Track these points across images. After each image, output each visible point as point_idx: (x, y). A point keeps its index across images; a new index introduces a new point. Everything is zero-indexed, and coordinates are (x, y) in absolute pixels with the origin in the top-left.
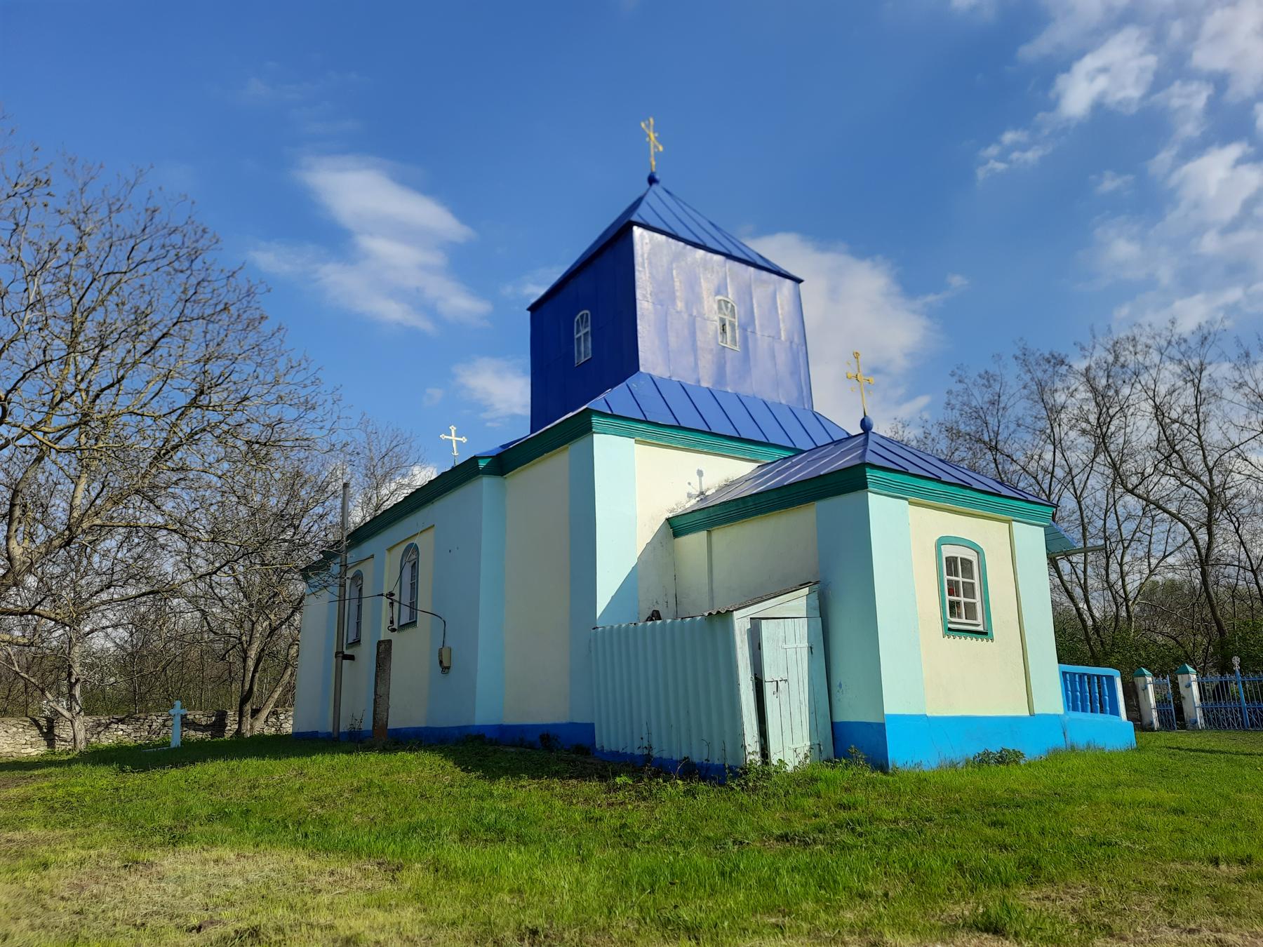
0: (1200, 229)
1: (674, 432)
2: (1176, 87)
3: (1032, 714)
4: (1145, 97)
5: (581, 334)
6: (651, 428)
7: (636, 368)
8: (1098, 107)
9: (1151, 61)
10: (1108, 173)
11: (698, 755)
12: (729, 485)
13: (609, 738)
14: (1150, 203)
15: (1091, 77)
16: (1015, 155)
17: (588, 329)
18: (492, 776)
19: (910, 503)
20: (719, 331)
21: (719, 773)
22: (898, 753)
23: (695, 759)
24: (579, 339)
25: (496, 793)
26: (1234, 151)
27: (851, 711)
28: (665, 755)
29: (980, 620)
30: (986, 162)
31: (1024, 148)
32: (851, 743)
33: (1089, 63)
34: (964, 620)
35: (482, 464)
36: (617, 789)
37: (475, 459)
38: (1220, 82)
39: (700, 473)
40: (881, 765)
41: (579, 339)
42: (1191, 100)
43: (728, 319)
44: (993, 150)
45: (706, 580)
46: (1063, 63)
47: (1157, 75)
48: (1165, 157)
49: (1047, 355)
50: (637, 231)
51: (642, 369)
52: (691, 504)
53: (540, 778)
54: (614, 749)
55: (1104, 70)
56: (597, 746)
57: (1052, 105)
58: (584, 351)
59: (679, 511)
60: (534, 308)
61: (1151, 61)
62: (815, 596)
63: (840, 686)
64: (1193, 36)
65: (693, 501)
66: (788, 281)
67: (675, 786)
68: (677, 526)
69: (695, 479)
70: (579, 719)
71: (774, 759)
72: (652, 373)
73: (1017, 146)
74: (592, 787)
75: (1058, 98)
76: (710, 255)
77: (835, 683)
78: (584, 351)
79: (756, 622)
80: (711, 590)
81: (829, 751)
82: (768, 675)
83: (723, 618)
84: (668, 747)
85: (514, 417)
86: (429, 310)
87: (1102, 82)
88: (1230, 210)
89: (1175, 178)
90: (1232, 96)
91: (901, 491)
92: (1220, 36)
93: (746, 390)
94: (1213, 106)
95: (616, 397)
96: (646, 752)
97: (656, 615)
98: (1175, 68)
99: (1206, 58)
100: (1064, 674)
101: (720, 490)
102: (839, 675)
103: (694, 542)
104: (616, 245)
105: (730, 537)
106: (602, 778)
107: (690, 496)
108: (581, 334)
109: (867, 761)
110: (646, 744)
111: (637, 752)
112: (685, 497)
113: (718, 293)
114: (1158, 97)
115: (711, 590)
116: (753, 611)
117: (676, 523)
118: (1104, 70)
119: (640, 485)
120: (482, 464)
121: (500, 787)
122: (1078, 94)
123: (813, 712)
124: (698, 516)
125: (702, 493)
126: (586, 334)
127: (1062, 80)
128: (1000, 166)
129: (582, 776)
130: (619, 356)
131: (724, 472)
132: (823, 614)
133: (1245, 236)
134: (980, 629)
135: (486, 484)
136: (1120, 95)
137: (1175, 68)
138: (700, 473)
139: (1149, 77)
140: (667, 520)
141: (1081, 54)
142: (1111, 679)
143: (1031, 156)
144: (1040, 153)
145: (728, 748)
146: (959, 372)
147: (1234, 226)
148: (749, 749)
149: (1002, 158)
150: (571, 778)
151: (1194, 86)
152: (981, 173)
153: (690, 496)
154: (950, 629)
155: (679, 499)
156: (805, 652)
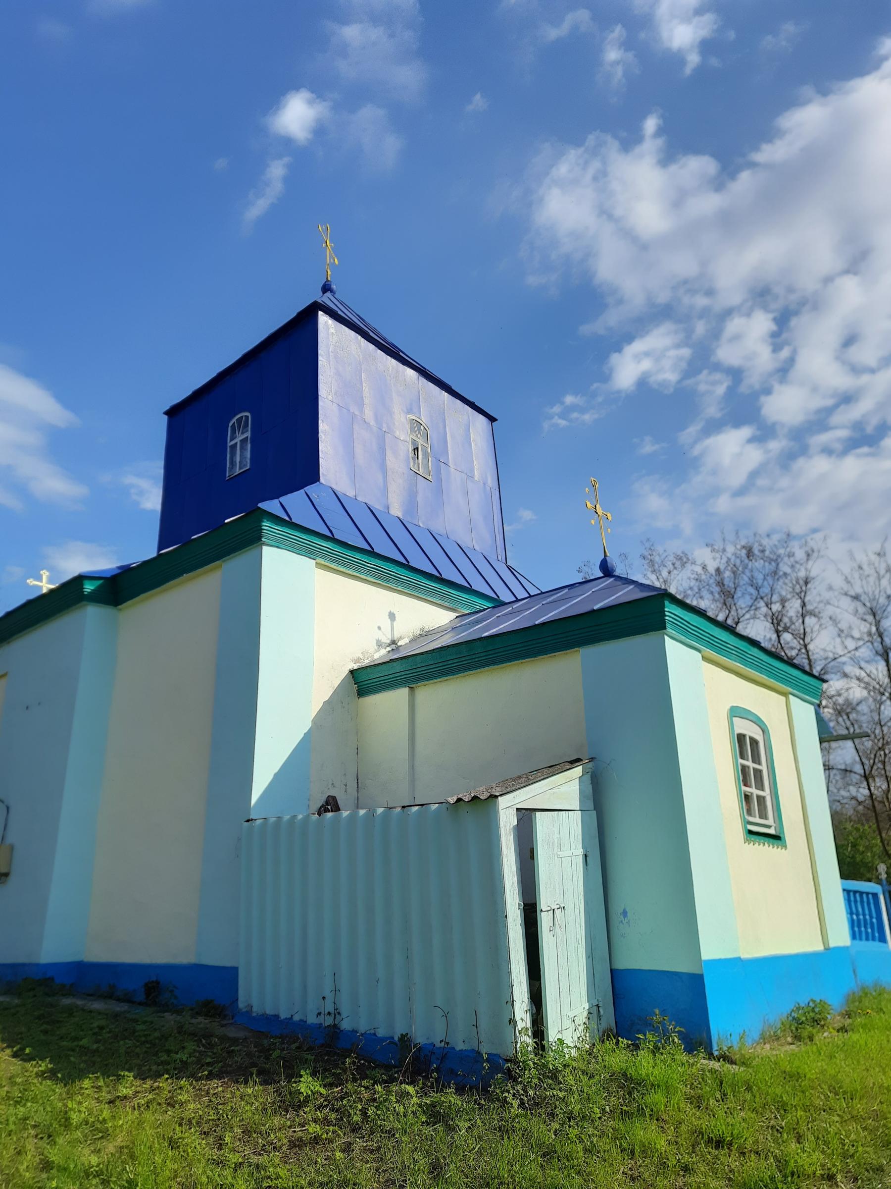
0: (715, 492)
1: (365, 558)
2: (704, 375)
3: (827, 949)
4: (679, 382)
5: (237, 440)
6: (337, 548)
7: (314, 477)
8: (642, 383)
9: (686, 352)
10: (648, 439)
11: (425, 1031)
12: (426, 634)
13: (265, 991)
14: (678, 465)
15: (638, 357)
16: (575, 415)
17: (248, 434)
18: (67, 1073)
19: (704, 658)
20: (411, 454)
21: (470, 1071)
22: (731, 1021)
23: (420, 1037)
24: (234, 447)
25: (75, 1118)
26: (746, 432)
27: (643, 954)
28: (363, 1027)
29: (770, 821)
30: (552, 418)
31: (582, 410)
32: (649, 1005)
33: (638, 346)
34: (757, 820)
35: (89, 587)
36: (297, 1104)
37: (80, 579)
38: (736, 374)
39: (392, 616)
40: (697, 1040)
41: (234, 447)
42: (713, 389)
43: (420, 442)
44: (557, 409)
45: (404, 754)
46: (619, 341)
47: (690, 363)
48: (693, 430)
49: (679, 553)
50: (323, 319)
51: (322, 480)
52: (380, 655)
53: (157, 1076)
54: (269, 1011)
55: (647, 354)
56: (241, 1005)
57: (606, 378)
58: (240, 457)
59: (366, 662)
60: (173, 413)
61: (686, 352)
62: (588, 777)
63: (625, 913)
64: (716, 334)
65: (383, 652)
66: (481, 417)
67: (403, 1096)
68: (364, 681)
69: (386, 623)
70: (215, 957)
71: (552, 1035)
72: (334, 487)
73: (574, 408)
74: (249, 1099)
75: (611, 370)
76: (401, 367)
77: (616, 909)
78: (240, 457)
79: (526, 816)
80: (412, 767)
81: (609, 1019)
82: (545, 901)
83: (482, 805)
84: (366, 1014)
85: (153, 511)
86: (21, 489)
87: (646, 365)
88: (737, 479)
89: (697, 450)
90: (743, 389)
91: (698, 638)
92: (737, 338)
93: (438, 527)
94: (731, 391)
95: (295, 503)
96: (329, 1021)
97: (331, 805)
98: (702, 359)
99: (726, 354)
100: (847, 891)
101: (414, 639)
102: (623, 896)
103: (390, 704)
104: (303, 325)
105: (439, 697)
106: (267, 1078)
107: (379, 644)
108: (237, 440)
109: (683, 1037)
110: (330, 1008)
111: (312, 1019)
112: (373, 646)
113: (410, 411)
114: (689, 382)
115: (412, 767)
116: (524, 797)
117: (363, 677)
118: (647, 354)
119: (316, 624)
120: (89, 587)
121: (87, 1099)
122: (628, 369)
123: (591, 956)
124: (398, 667)
125: (394, 642)
126: (244, 441)
127: (615, 358)
128: (563, 423)
129: (238, 1074)
130: (293, 458)
131: (421, 619)
132: (597, 801)
133: (748, 501)
134: (772, 831)
135: (92, 615)
136: (661, 377)
137: (702, 359)
138: (392, 616)
139: (684, 365)
140: (352, 672)
141: (629, 338)
142: (875, 895)
143: (587, 417)
144: (596, 416)
145: (484, 1024)
146: (585, 569)
147: (741, 492)
148: (520, 1025)
149: (563, 415)
150: (210, 1077)
151: (718, 376)
152: (546, 425)
153: (379, 644)
154: (751, 832)
155: (367, 648)
156: (580, 860)
